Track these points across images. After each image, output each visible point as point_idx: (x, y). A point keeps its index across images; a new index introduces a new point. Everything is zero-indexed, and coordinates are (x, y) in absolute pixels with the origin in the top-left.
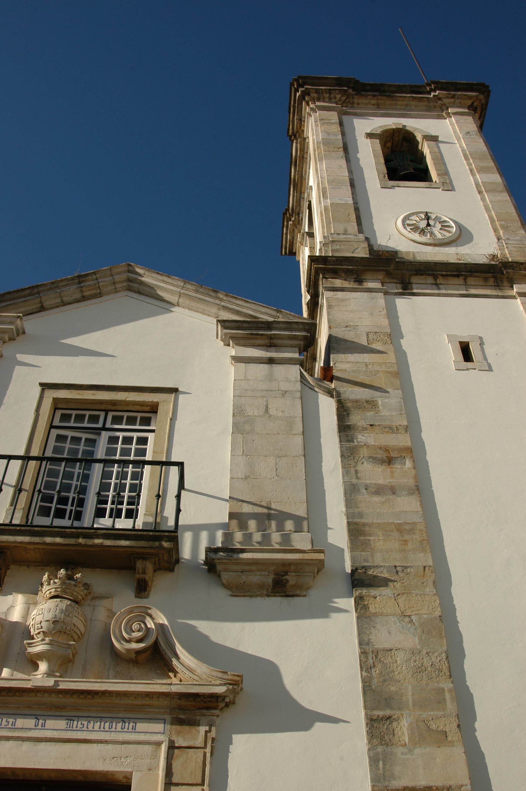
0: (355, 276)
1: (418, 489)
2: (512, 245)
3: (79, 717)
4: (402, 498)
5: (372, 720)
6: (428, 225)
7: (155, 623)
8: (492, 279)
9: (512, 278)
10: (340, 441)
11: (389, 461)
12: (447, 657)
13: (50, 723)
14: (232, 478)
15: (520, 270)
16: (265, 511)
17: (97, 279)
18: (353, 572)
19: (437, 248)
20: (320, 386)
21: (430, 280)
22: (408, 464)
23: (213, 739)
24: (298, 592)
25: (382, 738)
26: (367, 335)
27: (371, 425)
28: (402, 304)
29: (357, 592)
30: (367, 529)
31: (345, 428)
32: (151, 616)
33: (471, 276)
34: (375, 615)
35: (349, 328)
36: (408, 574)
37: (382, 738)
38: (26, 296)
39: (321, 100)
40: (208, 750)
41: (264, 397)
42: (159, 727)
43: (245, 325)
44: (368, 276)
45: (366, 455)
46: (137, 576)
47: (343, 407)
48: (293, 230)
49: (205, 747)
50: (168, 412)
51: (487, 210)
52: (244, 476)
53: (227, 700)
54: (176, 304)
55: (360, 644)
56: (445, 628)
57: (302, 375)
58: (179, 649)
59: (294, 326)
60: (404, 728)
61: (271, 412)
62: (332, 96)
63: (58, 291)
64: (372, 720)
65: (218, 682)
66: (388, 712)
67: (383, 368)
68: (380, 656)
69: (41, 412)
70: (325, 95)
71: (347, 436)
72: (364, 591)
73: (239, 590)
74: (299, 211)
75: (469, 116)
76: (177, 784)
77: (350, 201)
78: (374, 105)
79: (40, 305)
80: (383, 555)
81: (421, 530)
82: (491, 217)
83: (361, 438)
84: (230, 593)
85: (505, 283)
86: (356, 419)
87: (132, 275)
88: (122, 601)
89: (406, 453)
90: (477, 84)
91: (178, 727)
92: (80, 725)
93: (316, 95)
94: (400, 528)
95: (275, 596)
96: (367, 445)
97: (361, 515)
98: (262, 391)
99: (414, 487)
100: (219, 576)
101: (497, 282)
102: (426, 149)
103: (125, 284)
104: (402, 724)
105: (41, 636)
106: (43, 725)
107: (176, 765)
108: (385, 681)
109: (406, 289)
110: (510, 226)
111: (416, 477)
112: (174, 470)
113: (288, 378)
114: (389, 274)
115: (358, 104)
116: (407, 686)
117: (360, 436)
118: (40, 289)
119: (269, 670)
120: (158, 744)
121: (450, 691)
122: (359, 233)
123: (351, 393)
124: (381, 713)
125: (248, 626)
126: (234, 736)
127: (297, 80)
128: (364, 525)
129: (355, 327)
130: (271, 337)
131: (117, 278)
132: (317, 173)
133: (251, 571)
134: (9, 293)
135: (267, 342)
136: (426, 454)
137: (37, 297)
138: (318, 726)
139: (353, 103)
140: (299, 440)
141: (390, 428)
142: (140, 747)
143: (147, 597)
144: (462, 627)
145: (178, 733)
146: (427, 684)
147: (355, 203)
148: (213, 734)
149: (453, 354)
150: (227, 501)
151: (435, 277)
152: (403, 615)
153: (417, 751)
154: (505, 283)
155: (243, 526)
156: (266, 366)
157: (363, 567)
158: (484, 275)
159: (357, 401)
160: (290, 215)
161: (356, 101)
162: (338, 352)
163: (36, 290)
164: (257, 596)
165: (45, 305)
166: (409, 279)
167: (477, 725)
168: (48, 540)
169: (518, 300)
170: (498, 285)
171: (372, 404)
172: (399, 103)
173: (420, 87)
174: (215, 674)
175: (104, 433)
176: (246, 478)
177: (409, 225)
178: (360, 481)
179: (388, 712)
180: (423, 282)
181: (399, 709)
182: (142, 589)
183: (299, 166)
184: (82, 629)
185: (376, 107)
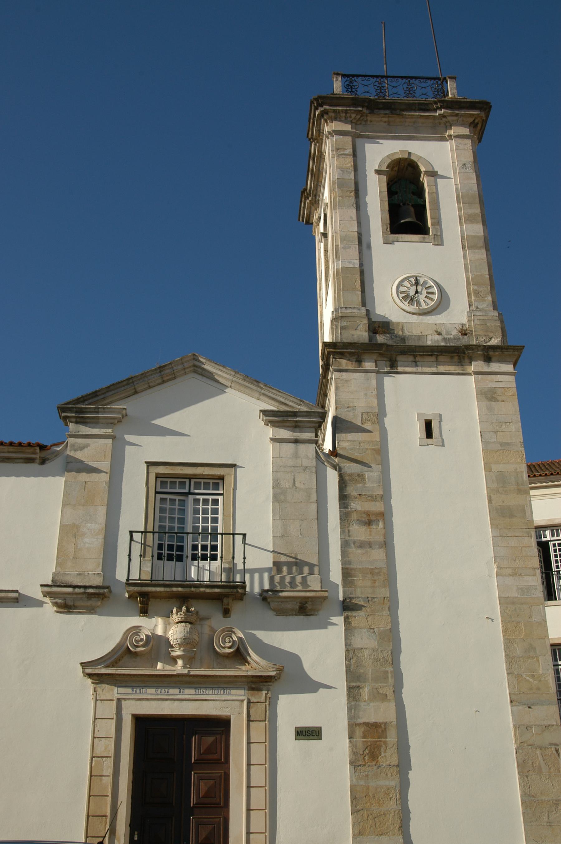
0: (356, 357)
1: (385, 544)
2: (479, 317)
3: (201, 688)
4: (375, 550)
5: (350, 688)
6: (417, 292)
7: (237, 637)
8: (457, 357)
9: (471, 357)
10: (340, 508)
11: (369, 523)
12: (392, 653)
13: (187, 691)
14: (274, 537)
15: (478, 351)
16: (294, 560)
17: (172, 367)
18: (344, 601)
19: (421, 317)
20: (328, 462)
21: (411, 358)
22: (381, 525)
23: (269, 698)
24: (312, 613)
25: (354, 698)
26: (362, 415)
27: (360, 495)
28: (388, 381)
29: (346, 614)
30: (353, 572)
31: (343, 498)
32: (235, 634)
33: (441, 355)
34: (355, 628)
35: (349, 409)
36: (374, 602)
37: (354, 698)
38: (124, 386)
39: (338, 119)
40: (267, 703)
41: (292, 472)
42: (242, 692)
43: (279, 414)
44: (366, 356)
45: (355, 519)
46: (224, 607)
47: (343, 480)
48: (310, 207)
49: (266, 702)
50: (231, 483)
51: (466, 271)
52: (282, 536)
53: (276, 678)
54: (229, 386)
55: (346, 645)
56: (391, 637)
57: (316, 451)
58: (250, 651)
59: (312, 414)
60: (365, 692)
61: (298, 484)
62: (348, 115)
63: (146, 379)
64: (350, 688)
65: (272, 669)
66: (358, 684)
67: (371, 447)
68: (356, 652)
69: (150, 485)
70: (341, 115)
71: (344, 504)
72: (349, 613)
73: (280, 612)
74: (316, 193)
75: (468, 139)
76: (253, 721)
77: (357, 266)
78: (385, 122)
79: (134, 391)
80: (362, 589)
81: (384, 573)
82: (467, 278)
83: (355, 505)
84: (275, 613)
85: (467, 360)
86: (351, 490)
87: (197, 363)
88: (217, 622)
89: (379, 518)
90: (479, 103)
91: (252, 692)
92: (202, 692)
93: (333, 115)
94: (372, 572)
95: (300, 615)
96: (356, 511)
97: (350, 563)
98: (291, 467)
99: (383, 543)
100: (269, 603)
101: (460, 359)
102: (425, 180)
103: (192, 369)
104: (365, 690)
105: (177, 646)
106: (183, 692)
107: (252, 712)
108: (357, 666)
109: (393, 367)
110: (481, 292)
111: (385, 535)
112: (239, 539)
113: (307, 456)
114: (381, 355)
115: (371, 121)
116: (369, 669)
117: (352, 504)
118: (134, 380)
119: (295, 659)
120: (242, 701)
121: (391, 672)
122: (362, 306)
123: (350, 468)
124: (354, 684)
125: (286, 633)
126: (280, 696)
127: (317, 99)
128: (352, 569)
129: (354, 408)
130: (296, 422)
131: (186, 365)
132: (332, 224)
133: (287, 602)
134: (113, 385)
135: (294, 424)
136: (392, 516)
137: (132, 386)
138: (321, 690)
139: (366, 121)
140: (314, 506)
141: (372, 496)
142: (233, 702)
143: (229, 617)
144: (402, 635)
145: (252, 695)
146: (380, 669)
147: (361, 265)
148: (269, 695)
149: (419, 430)
150: (271, 552)
151: (415, 356)
152: (370, 628)
153: (372, 704)
154: (467, 360)
155: (279, 571)
156: (292, 445)
157: (350, 598)
158: (450, 355)
159: (351, 475)
160: (308, 194)
161: (369, 119)
162: (341, 432)
163: (131, 381)
164: (290, 615)
165: (137, 390)
166: (396, 358)
167: (403, 690)
168: (175, 589)
169: (473, 377)
170: (461, 363)
171: (361, 477)
172: (407, 120)
173: (427, 104)
174: (270, 665)
175: (190, 496)
176: (282, 537)
177: (401, 293)
178: (350, 538)
179: (358, 684)
180: (406, 360)
181: (364, 682)
182: (226, 613)
183: (317, 162)
184: (197, 639)
185: (387, 124)
